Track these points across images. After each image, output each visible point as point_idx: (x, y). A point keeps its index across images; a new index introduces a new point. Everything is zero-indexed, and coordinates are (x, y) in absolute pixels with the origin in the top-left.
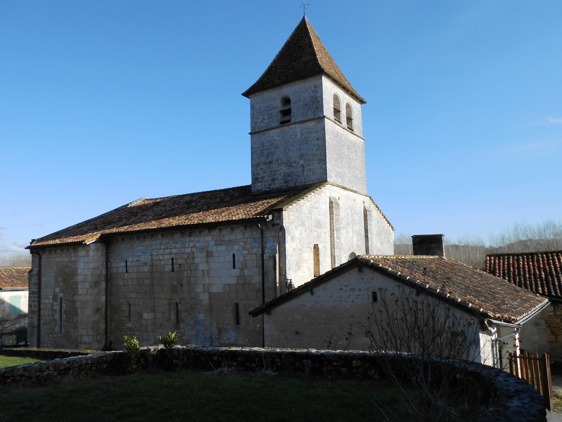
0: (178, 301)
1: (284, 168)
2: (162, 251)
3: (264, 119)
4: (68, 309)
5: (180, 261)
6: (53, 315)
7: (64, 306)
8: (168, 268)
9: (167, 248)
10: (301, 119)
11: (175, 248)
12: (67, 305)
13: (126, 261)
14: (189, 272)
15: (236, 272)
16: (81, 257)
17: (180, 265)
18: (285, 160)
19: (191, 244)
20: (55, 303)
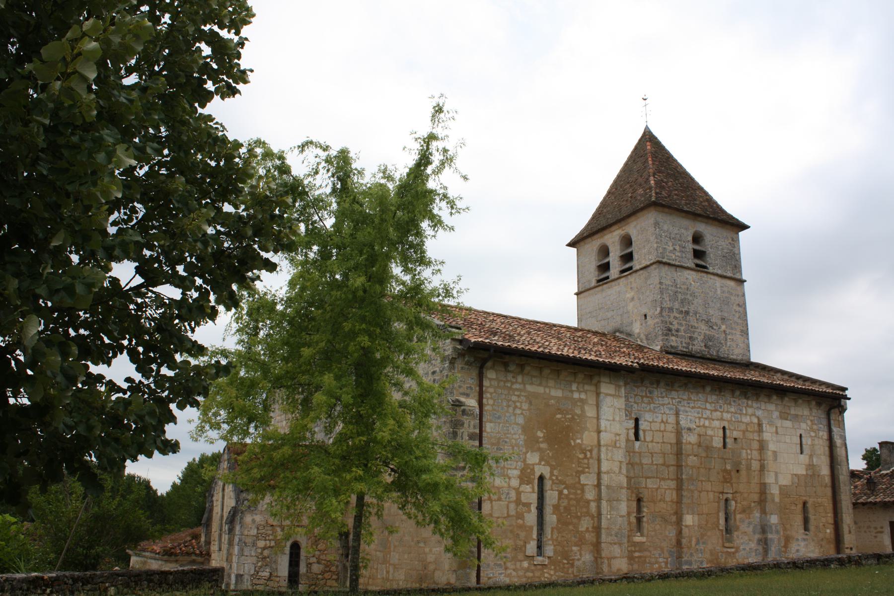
0: (730, 496)
1: (703, 327)
2: (708, 412)
3: (675, 249)
4: (565, 503)
5: (736, 434)
6: (520, 516)
7: (551, 496)
8: (717, 442)
9: (716, 410)
10: (719, 272)
11: (728, 412)
12: (560, 493)
13: (637, 421)
14: (749, 451)
15: (804, 459)
16: (607, 395)
17: (735, 439)
18: (704, 317)
19: (750, 411)
20: (528, 488)
